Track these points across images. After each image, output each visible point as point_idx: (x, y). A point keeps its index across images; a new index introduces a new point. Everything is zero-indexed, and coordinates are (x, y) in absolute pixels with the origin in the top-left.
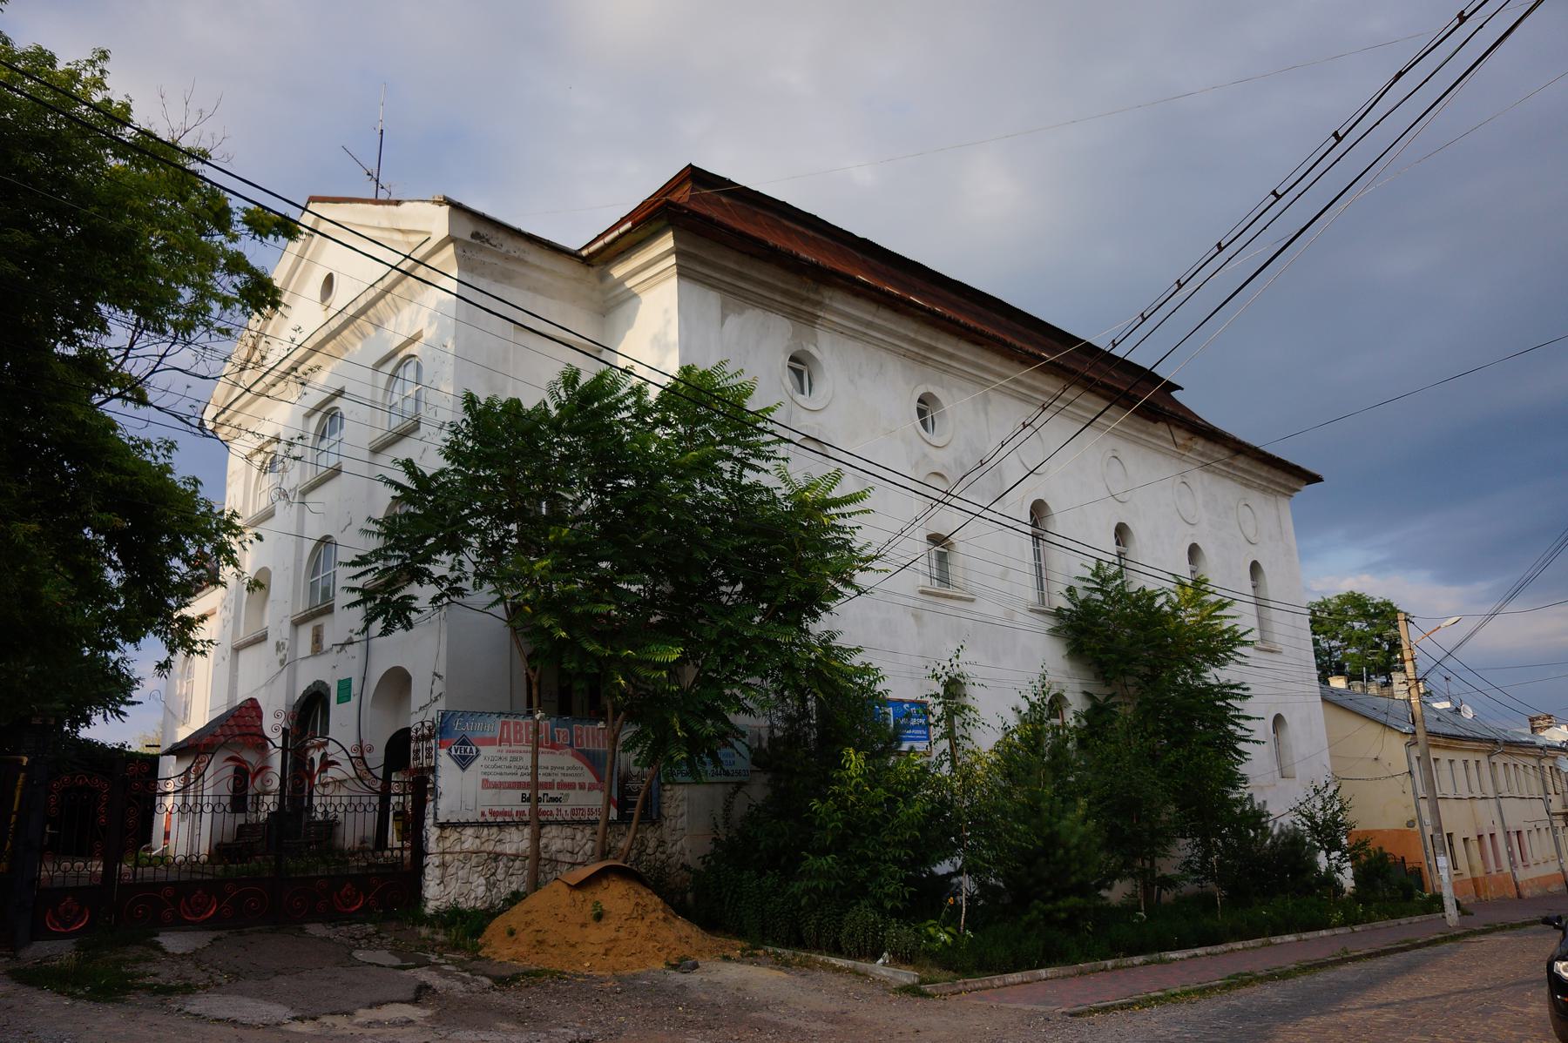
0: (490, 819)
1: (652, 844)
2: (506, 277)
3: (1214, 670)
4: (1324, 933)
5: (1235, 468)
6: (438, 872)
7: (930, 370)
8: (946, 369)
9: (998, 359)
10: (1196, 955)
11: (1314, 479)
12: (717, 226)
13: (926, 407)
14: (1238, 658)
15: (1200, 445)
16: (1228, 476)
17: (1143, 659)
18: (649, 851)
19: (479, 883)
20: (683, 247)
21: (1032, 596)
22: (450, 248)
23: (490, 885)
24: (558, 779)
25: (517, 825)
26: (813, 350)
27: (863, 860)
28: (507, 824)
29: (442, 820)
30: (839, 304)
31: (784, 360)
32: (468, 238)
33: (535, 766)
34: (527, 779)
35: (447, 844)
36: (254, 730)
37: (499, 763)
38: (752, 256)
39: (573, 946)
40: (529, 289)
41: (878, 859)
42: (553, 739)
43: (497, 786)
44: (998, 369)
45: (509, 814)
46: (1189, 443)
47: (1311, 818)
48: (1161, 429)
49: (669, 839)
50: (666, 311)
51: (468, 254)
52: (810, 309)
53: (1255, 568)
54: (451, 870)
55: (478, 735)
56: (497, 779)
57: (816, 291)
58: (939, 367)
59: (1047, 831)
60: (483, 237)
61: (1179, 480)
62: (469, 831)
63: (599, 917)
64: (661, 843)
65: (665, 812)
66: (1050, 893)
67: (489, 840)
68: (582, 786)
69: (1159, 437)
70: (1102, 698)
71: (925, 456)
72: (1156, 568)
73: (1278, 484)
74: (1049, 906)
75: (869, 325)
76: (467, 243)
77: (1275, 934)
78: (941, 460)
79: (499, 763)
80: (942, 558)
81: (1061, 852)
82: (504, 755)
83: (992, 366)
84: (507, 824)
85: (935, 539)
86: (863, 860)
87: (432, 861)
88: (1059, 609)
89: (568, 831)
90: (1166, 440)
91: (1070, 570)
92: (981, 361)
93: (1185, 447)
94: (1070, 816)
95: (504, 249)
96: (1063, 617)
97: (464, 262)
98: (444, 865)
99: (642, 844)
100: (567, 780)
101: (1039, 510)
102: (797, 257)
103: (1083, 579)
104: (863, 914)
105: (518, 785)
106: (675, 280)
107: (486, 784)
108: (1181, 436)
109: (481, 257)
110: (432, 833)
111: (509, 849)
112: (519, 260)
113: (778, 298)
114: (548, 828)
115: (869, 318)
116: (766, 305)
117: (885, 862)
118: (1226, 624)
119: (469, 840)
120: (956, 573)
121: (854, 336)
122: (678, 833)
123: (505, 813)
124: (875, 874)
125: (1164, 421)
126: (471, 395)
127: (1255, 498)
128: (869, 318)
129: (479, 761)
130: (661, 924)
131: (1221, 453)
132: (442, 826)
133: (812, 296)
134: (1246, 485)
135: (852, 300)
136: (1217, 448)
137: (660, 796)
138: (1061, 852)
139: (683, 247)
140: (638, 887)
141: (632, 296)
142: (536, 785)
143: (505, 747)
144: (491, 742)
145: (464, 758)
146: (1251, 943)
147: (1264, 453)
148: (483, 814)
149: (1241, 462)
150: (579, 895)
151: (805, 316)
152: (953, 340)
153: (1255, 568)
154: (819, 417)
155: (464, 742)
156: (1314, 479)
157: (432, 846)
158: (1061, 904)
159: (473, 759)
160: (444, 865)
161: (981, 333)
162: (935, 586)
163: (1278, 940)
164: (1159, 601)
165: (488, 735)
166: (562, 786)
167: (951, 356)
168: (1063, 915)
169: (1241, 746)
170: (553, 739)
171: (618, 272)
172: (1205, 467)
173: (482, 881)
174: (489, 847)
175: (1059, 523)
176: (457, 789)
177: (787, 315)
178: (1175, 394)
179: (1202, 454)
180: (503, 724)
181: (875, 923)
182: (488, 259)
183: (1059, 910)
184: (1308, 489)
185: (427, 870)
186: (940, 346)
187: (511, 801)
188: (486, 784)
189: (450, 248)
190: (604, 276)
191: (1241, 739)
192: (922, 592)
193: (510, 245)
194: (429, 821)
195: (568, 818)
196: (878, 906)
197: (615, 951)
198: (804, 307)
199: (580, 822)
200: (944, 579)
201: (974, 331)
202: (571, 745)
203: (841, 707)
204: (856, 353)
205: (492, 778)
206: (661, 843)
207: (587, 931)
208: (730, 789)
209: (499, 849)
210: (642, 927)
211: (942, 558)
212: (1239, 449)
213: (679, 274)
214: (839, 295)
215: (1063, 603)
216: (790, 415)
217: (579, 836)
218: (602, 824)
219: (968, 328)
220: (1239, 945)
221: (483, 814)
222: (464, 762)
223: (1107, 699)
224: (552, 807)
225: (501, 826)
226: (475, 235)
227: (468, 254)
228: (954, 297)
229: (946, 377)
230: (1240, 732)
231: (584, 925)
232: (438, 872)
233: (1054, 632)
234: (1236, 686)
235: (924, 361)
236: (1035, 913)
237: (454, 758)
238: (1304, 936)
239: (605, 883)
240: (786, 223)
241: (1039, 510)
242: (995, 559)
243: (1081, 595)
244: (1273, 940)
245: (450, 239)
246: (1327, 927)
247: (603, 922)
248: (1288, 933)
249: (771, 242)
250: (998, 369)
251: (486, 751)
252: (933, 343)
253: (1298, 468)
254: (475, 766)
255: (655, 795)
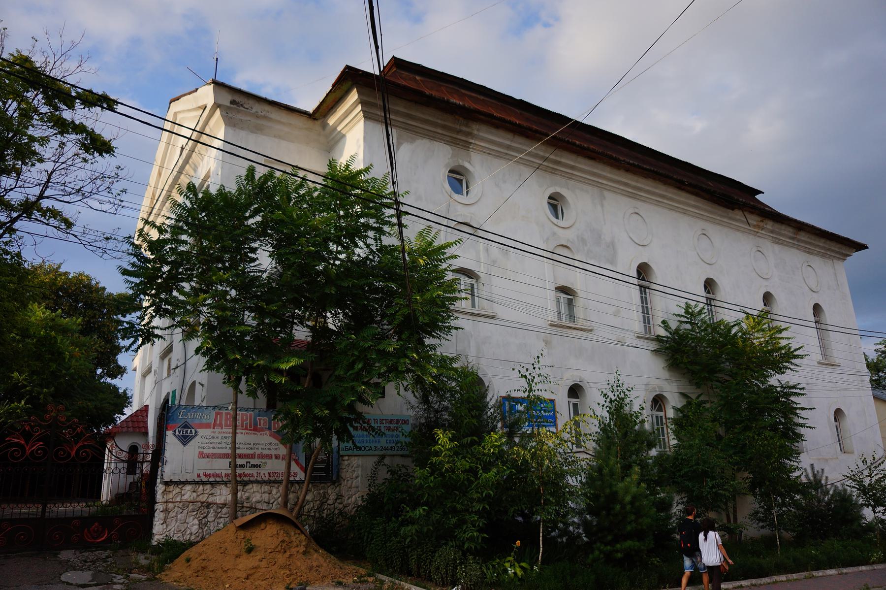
0: (204, 479)
1: (332, 497)
2: (257, 129)
3: (778, 376)
4: (864, 568)
5: (799, 241)
6: (162, 515)
7: (558, 178)
8: (570, 177)
9: (608, 169)
10: (741, 586)
11: (861, 247)
12: (407, 95)
13: (556, 204)
14: (792, 367)
15: (769, 225)
16: (793, 246)
17: (727, 372)
18: (330, 502)
19: (193, 525)
20: (365, 98)
21: (638, 327)
22: (218, 112)
23: (201, 525)
24: (258, 452)
25: (225, 483)
26: (467, 165)
27: (454, 511)
28: (218, 483)
29: (166, 480)
30: (484, 134)
31: (445, 172)
32: (228, 104)
33: (234, 442)
34: (230, 452)
35: (171, 496)
36: (141, 425)
37: (212, 441)
38: (416, 102)
39: (226, 571)
40: (275, 136)
41: (467, 510)
42: (255, 425)
43: (209, 456)
44: (609, 175)
45: (220, 476)
46: (761, 224)
47: (860, 483)
48: (738, 214)
49: (344, 493)
50: (358, 141)
51: (230, 115)
52: (463, 138)
53: (817, 308)
54: (172, 514)
55: (197, 421)
56: (210, 451)
57: (467, 126)
58: (564, 175)
59: (608, 491)
60: (237, 102)
61: (755, 249)
62: (188, 488)
63: (250, 550)
64: (339, 496)
65: (343, 475)
66: (609, 538)
67: (204, 494)
68: (277, 457)
69: (737, 220)
70: (694, 397)
71: (554, 234)
72: (736, 305)
73: (833, 251)
74: (609, 547)
75: (509, 147)
76: (229, 108)
77: (818, 569)
78: (565, 236)
79: (212, 441)
80: (570, 303)
81: (618, 507)
82: (217, 435)
83: (604, 174)
84: (218, 483)
85: (563, 290)
86: (454, 511)
87: (159, 507)
88: (658, 336)
89: (266, 488)
90: (742, 222)
91: (667, 309)
92: (595, 171)
93: (758, 227)
94: (628, 479)
95: (254, 111)
96: (663, 341)
97: (229, 122)
98: (166, 511)
99: (324, 497)
100: (265, 452)
101: (643, 271)
102: (448, 102)
103: (678, 315)
104: (449, 552)
105: (225, 456)
106: (362, 123)
107: (201, 455)
108: (754, 219)
109: (239, 116)
110: (160, 488)
111: (219, 500)
112: (265, 117)
113: (439, 131)
114: (250, 486)
115: (508, 143)
116: (432, 136)
117: (470, 514)
118: (783, 343)
119: (188, 493)
120: (579, 312)
121: (499, 156)
122: (353, 490)
123: (216, 475)
124: (463, 522)
125: (739, 209)
126: (556, 288)
127: (817, 262)
128: (508, 143)
129: (197, 439)
130: (300, 556)
131: (788, 231)
132: (167, 484)
133: (464, 128)
134: (809, 253)
135: (494, 130)
136: (783, 227)
137: (339, 464)
138: (618, 507)
139: (365, 98)
140: (288, 527)
141: (344, 136)
142: (235, 456)
143: (217, 430)
144: (208, 426)
145: (185, 437)
146: (795, 576)
147: (820, 230)
148: (199, 476)
149: (803, 236)
150: (241, 534)
151: (462, 143)
152: (573, 157)
153: (817, 308)
154: (472, 209)
155: (186, 426)
156: (861, 247)
157: (159, 497)
158: (618, 546)
159: (192, 437)
160: (166, 511)
161: (593, 151)
162: (565, 321)
163: (820, 573)
164: (734, 331)
165: (205, 421)
166: (261, 456)
167: (573, 168)
168: (619, 555)
169: (802, 431)
170: (255, 425)
171: (332, 121)
172: (777, 241)
173: (196, 522)
174: (203, 498)
175: (660, 275)
176: (179, 459)
177: (447, 143)
178: (758, 197)
179: (772, 232)
180: (217, 414)
181: (455, 560)
182: (244, 118)
183: (617, 551)
184: (857, 255)
185: (156, 514)
186: (563, 160)
187: (222, 467)
188: (201, 455)
189: (218, 112)
190: (325, 125)
191: (802, 425)
192: (551, 325)
193: (257, 108)
194: (159, 481)
195: (266, 479)
196: (460, 547)
197: (255, 576)
198: (459, 137)
199: (275, 482)
200: (572, 316)
201: (588, 149)
202: (269, 429)
203: (462, 400)
204: (501, 167)
205: (206, 451)
206: (339, 496)
207: (239, 560)
208: (376, 459)
209: (210, 500)
210: (281, 559)
211: (570, 303)
212: (800, 227)
213: (365, 117)
214: (484, 128)
215: (662, 332)
216: (448, 208)
217: (274, 491)
218: (284, 483)
219: (583, 148)
220: (783, 578)
221: (199, 476)
222: (185, 440)
223: (698, 397)
224: (254, 471)
225: (213, 484)
226: (233, 102)
227: (230, 115)
228: (588, 136)
229: (571, 183)
230: (801, 421)
231: (238, 556)
232: (162, 515)
233: (656, 352)
234: (794, 387)
235: (553, 171)
236: (597, 553)
237: (178, 437)
238: (845, 570)
239: (263, 526)
240: (463, 91)
241: (643, 271)
242: (611, 306)
243: (673, 325)
244: (815, 573)
245: (216, 105)
246: (866, 562)
247: (253, 554)
248: (831, 568)
249: (428, 92)
250: (609, 175)
251: (202, 432)
252: (558, 159)
253: (847, 240)
254: (194, 444)
255: (335, 463)
